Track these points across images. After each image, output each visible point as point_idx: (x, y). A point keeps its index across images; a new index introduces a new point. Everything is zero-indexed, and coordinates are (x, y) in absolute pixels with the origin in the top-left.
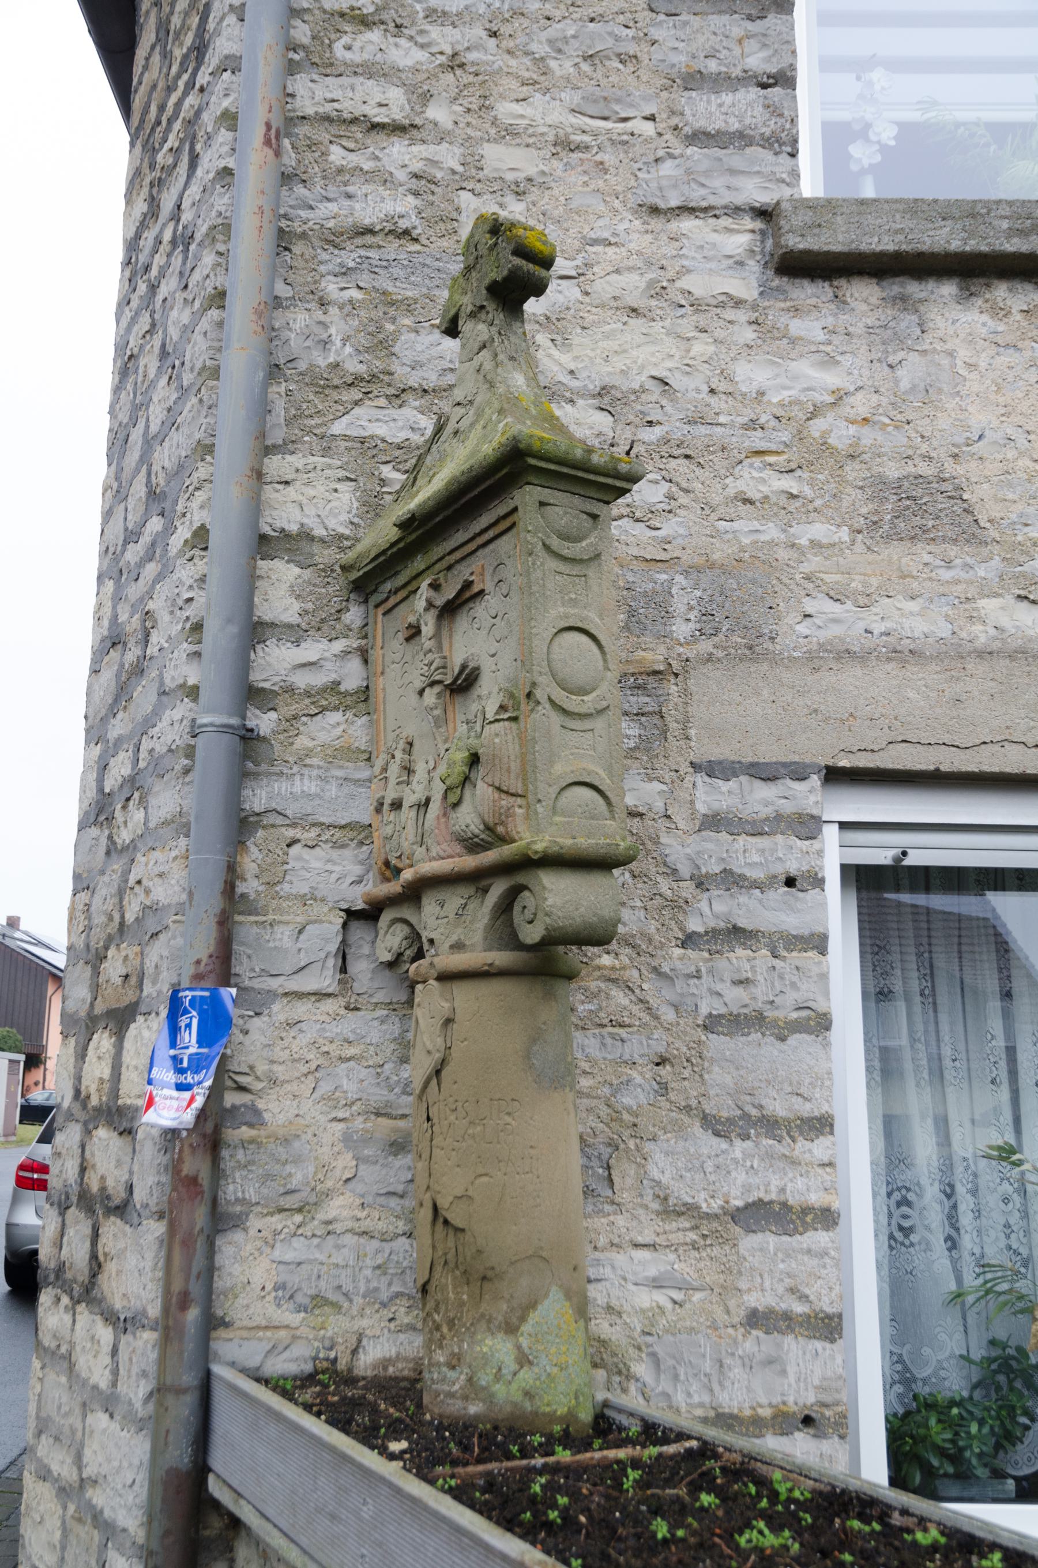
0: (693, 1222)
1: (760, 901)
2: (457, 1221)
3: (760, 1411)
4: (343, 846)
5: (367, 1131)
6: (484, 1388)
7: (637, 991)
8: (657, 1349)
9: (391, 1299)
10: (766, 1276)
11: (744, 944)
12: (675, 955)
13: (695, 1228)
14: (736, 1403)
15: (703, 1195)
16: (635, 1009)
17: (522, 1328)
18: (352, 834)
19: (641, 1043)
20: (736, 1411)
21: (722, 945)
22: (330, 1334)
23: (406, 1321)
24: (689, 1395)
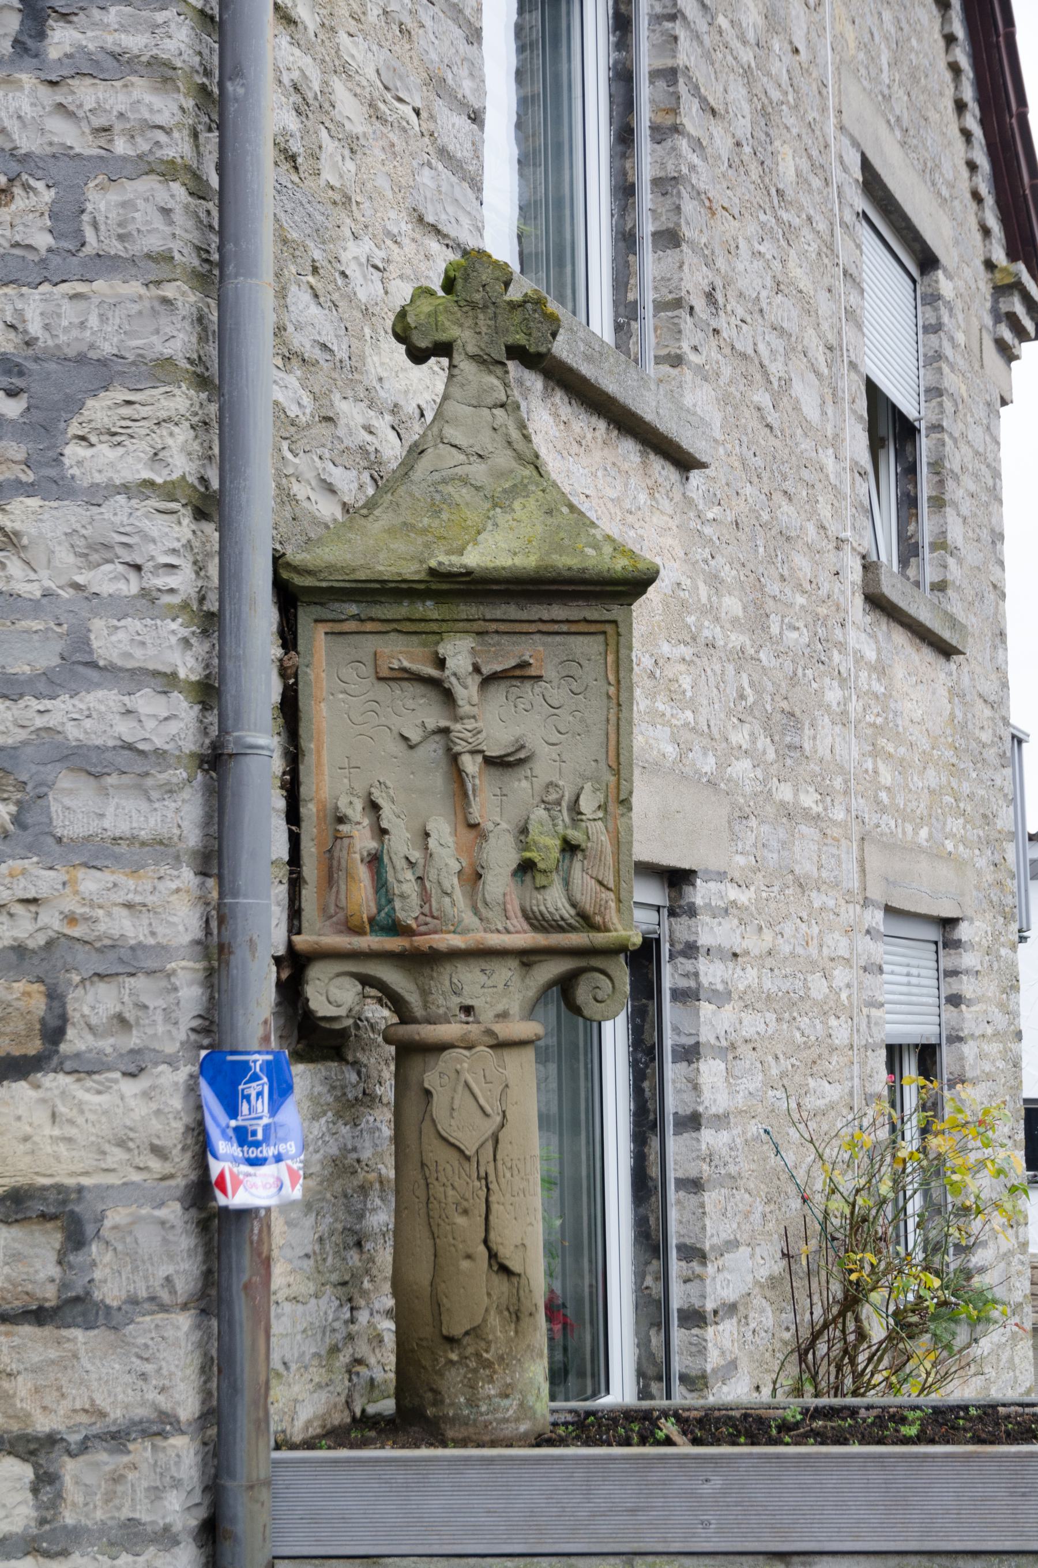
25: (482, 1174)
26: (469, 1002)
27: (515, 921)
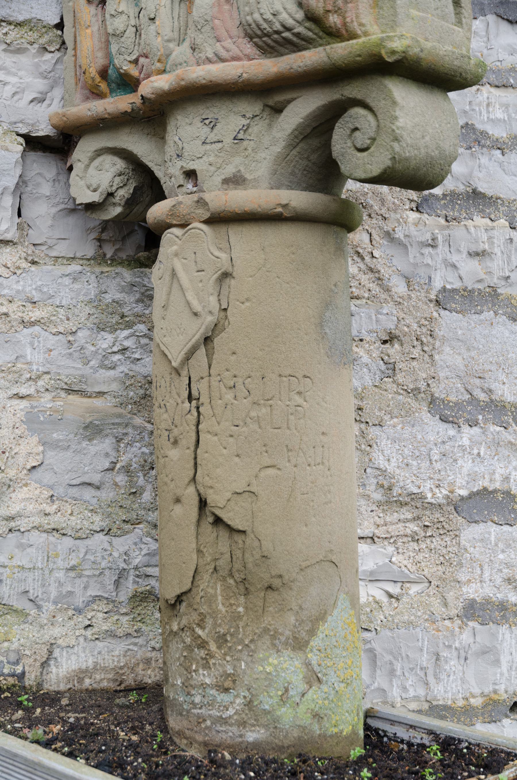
0: (416, 512)
1: (501, 164)
2: (237, 523)
3: (472, 701)
4: (20, 51)
5: (57, 411)
6: (266, 712)
7: (367, 258)
8: (374, 645)
9: (88, 604)
10: (486, 567)
11: (482, 211)
12: (410, 220)
13: (414, 519)
14: (450, 694)
15: (429, 484)
16: (364, 279)
17: (312, 643)
18: (33, 36)
19: (370, 318)
20: (449, 703)
21: (459, 211)
22: (15, 646)
23: (105, 628)
24: (405, 689)
25: (195, 393)
26: (191, 166)
27: (228, 43)
